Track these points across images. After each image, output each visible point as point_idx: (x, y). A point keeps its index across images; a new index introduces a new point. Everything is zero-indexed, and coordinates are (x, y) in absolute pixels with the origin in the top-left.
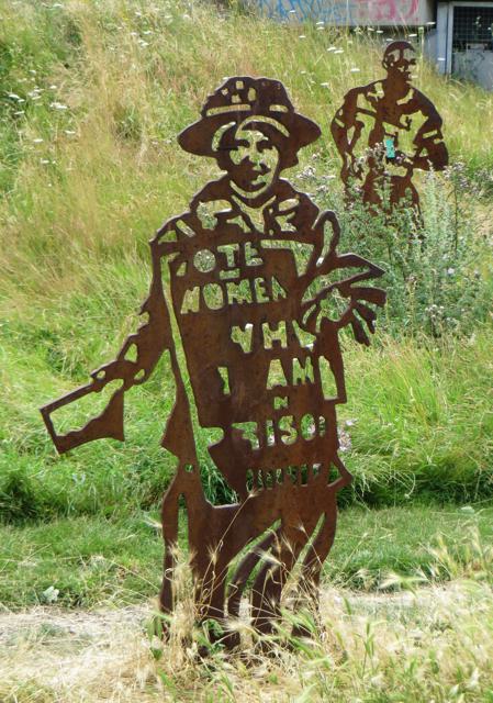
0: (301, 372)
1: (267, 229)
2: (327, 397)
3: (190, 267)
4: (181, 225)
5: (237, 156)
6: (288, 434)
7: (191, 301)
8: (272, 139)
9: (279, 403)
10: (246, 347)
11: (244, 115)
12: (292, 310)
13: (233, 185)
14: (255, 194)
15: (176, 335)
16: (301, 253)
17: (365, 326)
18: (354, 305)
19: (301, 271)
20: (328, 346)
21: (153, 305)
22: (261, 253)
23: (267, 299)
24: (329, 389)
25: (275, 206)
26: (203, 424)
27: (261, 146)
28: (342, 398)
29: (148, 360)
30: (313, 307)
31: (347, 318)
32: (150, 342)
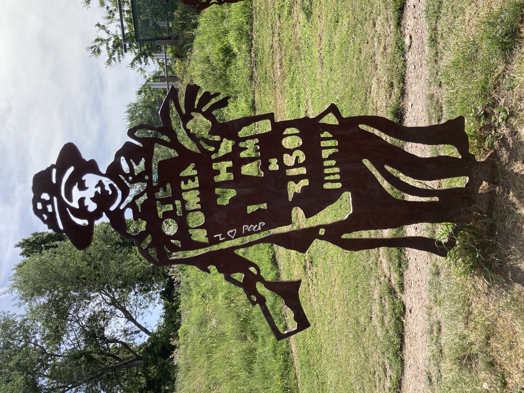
0: (250, 149)
1: (144, 181)
2: (269, 129)
3: (174, 237)
4: (144, 246)
5: (92, 207)
6: (297, 158)
7: (201, 236)
8: (77, 180)
9: (274, 166)
10: (232, 193)
11: (60, 200)
12: (204, 163)
13: (112, 208)
14: (119, 192)
15: (225, 245)
16: (161, 153)
17: (213, 101)
18: (199, 110)
19: (173, 153)
20: (230, 129)
21: (202, 263)
22: (162, 183)
23: (196, 178)
24: (265, 127)
25: (126, 176)
26: (288, 221)
27: (82, 187)
28: (270, 116)
29: (244, 265)
30: (202, 143)
31: (208, 115)
32: (229, 263)
